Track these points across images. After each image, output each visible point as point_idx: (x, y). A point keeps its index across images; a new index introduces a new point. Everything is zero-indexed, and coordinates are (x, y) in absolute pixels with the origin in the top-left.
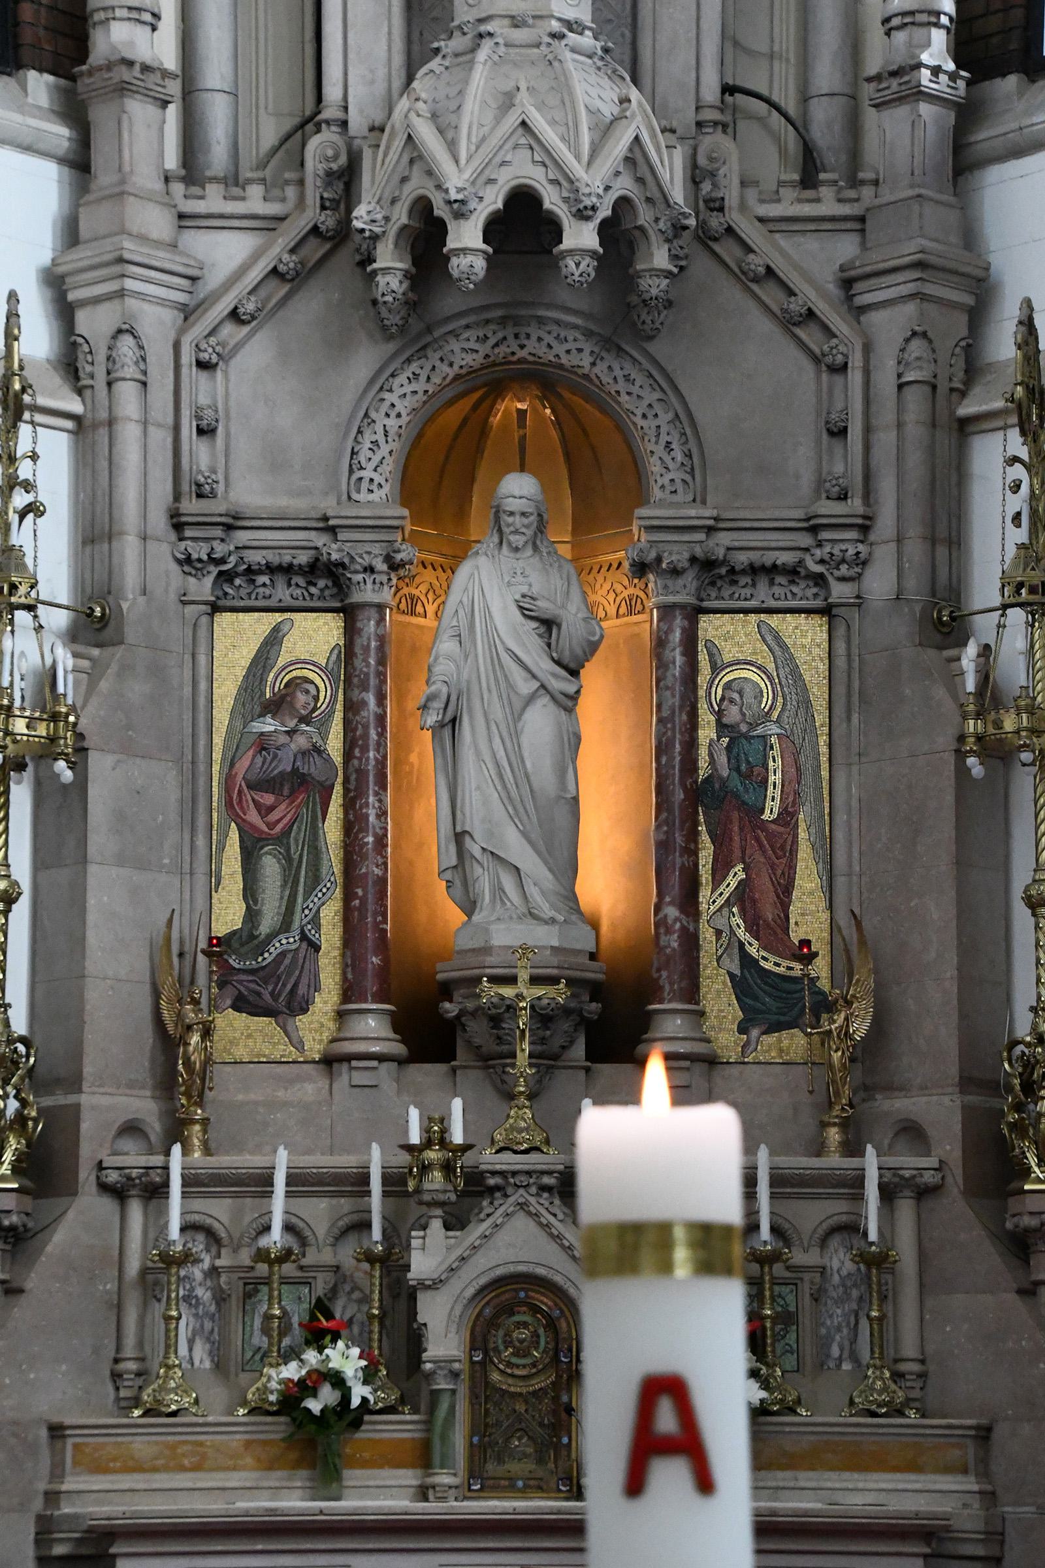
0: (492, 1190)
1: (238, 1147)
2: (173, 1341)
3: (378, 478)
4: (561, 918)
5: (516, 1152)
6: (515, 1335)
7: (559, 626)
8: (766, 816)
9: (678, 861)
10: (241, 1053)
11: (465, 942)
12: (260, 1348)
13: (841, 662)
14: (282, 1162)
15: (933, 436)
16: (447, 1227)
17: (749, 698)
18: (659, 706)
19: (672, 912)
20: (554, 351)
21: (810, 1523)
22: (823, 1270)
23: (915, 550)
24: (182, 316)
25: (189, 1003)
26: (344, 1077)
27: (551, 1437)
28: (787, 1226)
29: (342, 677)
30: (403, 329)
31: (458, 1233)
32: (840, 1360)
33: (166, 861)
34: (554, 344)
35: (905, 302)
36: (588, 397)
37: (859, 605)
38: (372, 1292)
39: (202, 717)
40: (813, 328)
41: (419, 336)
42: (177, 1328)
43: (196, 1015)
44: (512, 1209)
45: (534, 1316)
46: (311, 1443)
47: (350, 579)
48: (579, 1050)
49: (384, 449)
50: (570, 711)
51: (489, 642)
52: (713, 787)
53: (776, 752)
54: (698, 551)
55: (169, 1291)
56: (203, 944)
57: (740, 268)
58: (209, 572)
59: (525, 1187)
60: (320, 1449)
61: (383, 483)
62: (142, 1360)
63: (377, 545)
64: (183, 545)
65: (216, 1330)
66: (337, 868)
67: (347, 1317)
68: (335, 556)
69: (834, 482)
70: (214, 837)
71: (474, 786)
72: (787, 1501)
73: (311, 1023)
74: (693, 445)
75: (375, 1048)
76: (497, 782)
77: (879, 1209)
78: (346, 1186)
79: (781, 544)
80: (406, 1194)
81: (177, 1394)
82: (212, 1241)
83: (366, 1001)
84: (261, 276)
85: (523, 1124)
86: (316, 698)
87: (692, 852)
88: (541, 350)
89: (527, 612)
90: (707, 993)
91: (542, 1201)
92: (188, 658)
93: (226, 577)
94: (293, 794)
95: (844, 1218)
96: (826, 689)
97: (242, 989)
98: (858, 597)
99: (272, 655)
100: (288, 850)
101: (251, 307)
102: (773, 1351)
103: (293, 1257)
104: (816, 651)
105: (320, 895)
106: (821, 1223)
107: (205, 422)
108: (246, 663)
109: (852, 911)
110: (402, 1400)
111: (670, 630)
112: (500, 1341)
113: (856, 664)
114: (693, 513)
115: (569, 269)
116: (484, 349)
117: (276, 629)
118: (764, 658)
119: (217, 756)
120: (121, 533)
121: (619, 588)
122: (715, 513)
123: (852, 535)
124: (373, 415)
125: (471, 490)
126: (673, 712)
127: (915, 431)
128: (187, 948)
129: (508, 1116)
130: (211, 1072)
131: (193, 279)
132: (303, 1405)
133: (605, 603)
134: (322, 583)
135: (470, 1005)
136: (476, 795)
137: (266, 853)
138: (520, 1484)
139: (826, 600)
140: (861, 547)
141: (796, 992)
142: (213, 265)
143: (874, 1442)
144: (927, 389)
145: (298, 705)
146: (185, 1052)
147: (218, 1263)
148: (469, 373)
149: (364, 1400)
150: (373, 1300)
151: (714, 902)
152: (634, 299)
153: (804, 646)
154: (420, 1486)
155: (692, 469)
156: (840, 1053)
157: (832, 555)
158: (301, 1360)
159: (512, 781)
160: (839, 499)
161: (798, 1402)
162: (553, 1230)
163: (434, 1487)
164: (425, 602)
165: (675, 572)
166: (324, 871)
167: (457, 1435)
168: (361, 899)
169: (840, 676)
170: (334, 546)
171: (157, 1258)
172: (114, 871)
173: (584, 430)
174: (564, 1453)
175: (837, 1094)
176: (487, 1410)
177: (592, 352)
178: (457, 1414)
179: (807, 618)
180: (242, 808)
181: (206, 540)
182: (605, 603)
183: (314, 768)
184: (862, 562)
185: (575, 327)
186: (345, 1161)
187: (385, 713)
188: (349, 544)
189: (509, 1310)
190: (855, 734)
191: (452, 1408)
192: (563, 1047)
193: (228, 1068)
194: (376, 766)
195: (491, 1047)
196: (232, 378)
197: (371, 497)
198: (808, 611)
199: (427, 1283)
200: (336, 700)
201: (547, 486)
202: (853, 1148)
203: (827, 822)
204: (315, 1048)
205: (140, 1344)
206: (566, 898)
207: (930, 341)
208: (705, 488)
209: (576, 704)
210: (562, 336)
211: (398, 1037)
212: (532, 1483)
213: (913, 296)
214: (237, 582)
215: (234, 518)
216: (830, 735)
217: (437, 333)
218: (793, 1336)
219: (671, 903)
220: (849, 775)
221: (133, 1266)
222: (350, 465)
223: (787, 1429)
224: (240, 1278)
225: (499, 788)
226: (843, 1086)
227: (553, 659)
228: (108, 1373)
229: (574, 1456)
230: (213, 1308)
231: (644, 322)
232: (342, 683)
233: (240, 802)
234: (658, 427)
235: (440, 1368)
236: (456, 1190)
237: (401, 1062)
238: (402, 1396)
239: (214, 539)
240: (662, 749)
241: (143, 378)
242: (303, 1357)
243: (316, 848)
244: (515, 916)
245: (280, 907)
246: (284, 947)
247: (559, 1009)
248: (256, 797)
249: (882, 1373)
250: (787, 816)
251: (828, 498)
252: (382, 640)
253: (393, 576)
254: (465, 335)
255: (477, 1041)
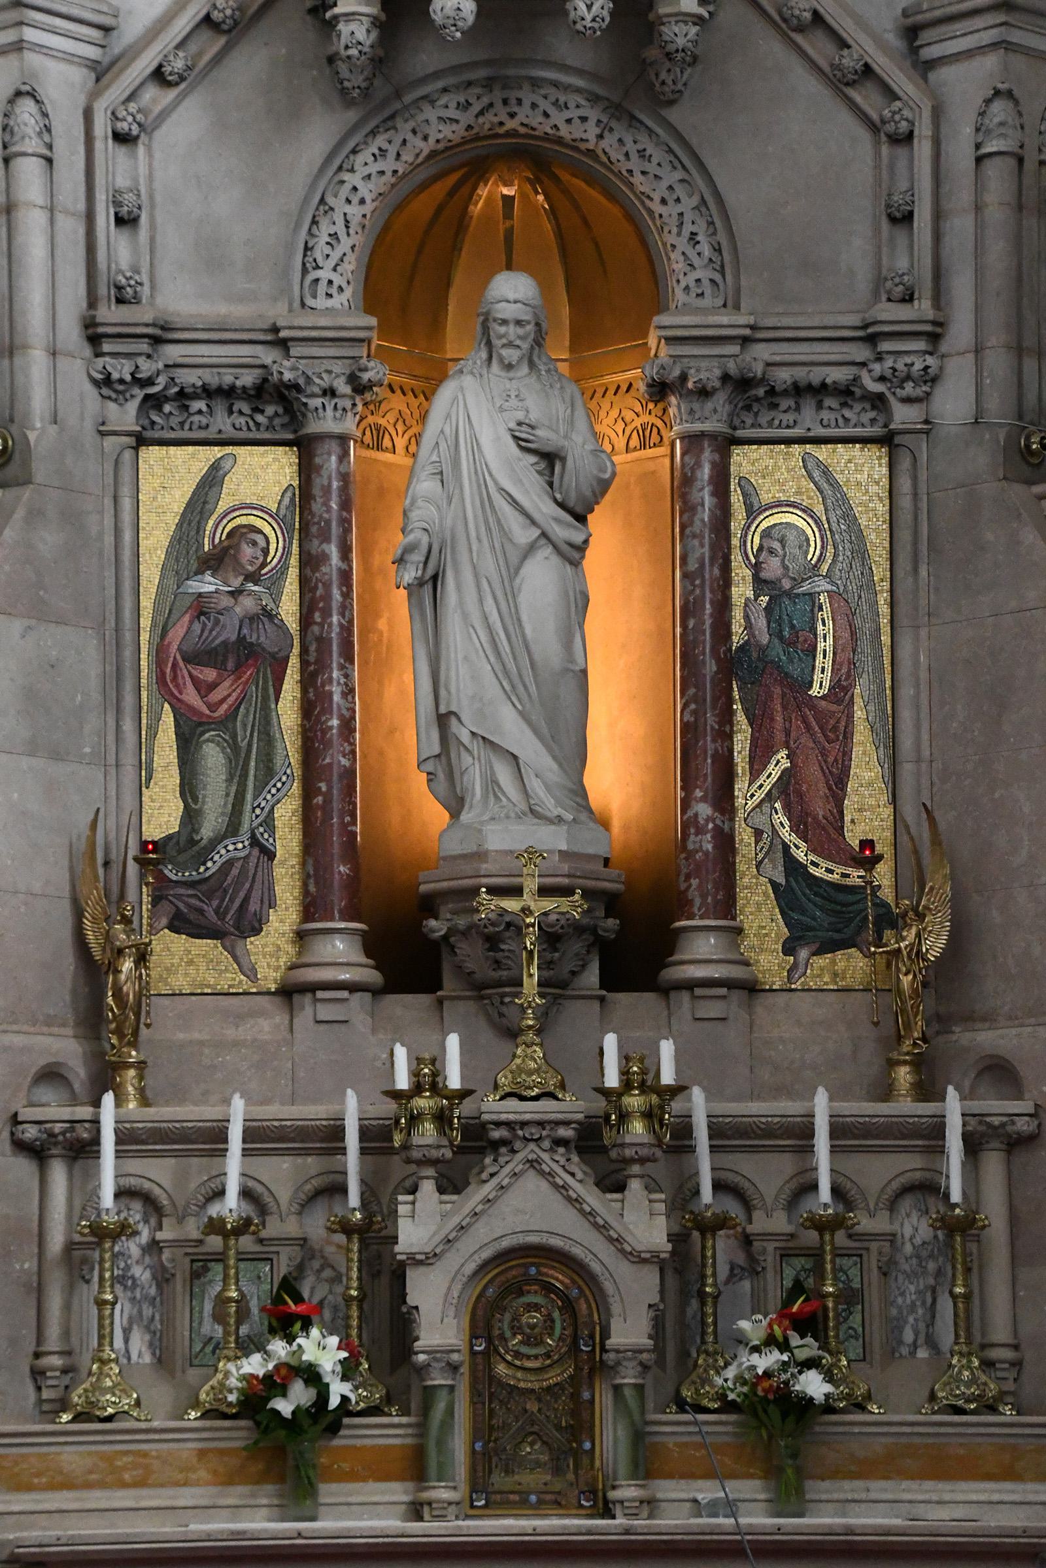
0: (495, 1145)
1: (180, 1095)
2: (108, 1330)
3: (338, 280)
4: (569, 817)
5: (523, 1098)
6: (524, 1320)
7: (563, 460)
8: (815, 691)
9: (710, 747)
10: (180, 982)
11: (453, 846)
12: (211, 1338)
13: (905, 502)
14: (238, 1112)
15: (1019, 224)
16: (441, 1190)
17: (792, 549)
18: (684, 559)
19: (704, 810)
20: (552, 121)
21: (892, 1542)
22: (892, 1238)
23: (998, 362)
24: (93, 76)
25: (120, 923)
26: (307, 1010)
27: (570, 1442)
28: (849, 1185)
29: (297, 524)
30: (366, 93)
31: (454, 1197)
32: (915, 1346)
33: (87, 750)
34: (551, 110)
35: (984, 53)
36: (592, 179)
37: (927, 432)
38: (349, 1269)
39: (127, 574)
40: (870, 87)
41: (385, 103)
42: (112, 1315)
43: (128, 937)
44: (521, 1166)
45: (546, 1296)
46: (280, 1451)
47: (305, 404)
48: (592, 977)
49: (345, 243)
50: (576, 564)
51: (478, 480)
52: (749, 657)
53: (826, 613)
54: (732, 367)
55: (102, 1270)
56: (133, 851)
57: (780, 13)
58: (132, 396)
59: (536, 1140)
60: (291, 1462)
61: (344, 285)
62: (68, 1353)
63: (339, 362)
64: (100, 361)
65: (157, 1317)
66: (295, 758)
67: (315, 1301)
68: (288, 376)
69: (897, 280)
70: (144, 721)
71: (460, 656)
72: (858, 1516)
73: (264, 946)
74: (722, 237)
75: (345, 976)
76: (489, 652)
77: (963, 1164)
78: (313, 1141)
79: (833, 358)
80: (391, 1151)
81: (114, 1395)
82: (151, 1209)
83: (332, 919)
84: (191, 25)
85: (532, 1065)
86: (266, 552)
87: (726, 735)
88: (536, 120)
89: (523, 444)
90: (744, 906)
91: (557, 1158)
92: (108, 502)
93: (153, 402)
94: (239, 667)
95: (918, 1175)
96: (886, 535)
97: (181, 906)
98: (927, 422)
99: (211, 498)
100: (234, 736)
101: (179, 64)
102: (837, 1336)
103: (253, 1228)
104: (873, 489)
105: (274, 791)
106: (890, 1181)
107: (126, 208)
108: (178, 507)
109: (924, 804)
110: (388, 1399)
111: (698, 464)
112: (506, 1326)
113: (924, 505)
114: (725, 320)
115: (579, 13)
116: (466, 118)
117: (215, 467)
118: (810, 498)
119: (146, 622)
120: (26, 347)
121: (629, 415)
122: (751, 320)
123: (921, 345)
124: (330, 200)
125: (446, 298)
126: (702, 565)
127: (997, 213)
128: (113, 856)
129: (514, 1056)
130: (148, 1005)
131: (106, 29)
132: (268, 1407)
133: (613, 435)
134: (270, 410)
135: (462, 922)
136: (463, 670)
137: (208, 740)
138: (533, 1498)
139: (886, 426)
140: (930, 360)
141: (858, 902)
142: (130, 12)
143: (961, 1445)
144: (1012, 162)
145: (244, 561)
146: (115, 982)
147: (160, 1236)
148: (447, 149)
149: (345, 1399)
150: (349, 1279)
151: (752, 796)
152: (652, 53)
153: (859, 484)
154: (413, 1503)
155: (722, 266)
156: (910, 977)
157: (894, 370)
158: (266, 1352)
159: (508, 649)
160: (903, 300)
161: (868, 1397)
162: (571, 1193)
163: (430, 1504)
164: (394, 433)
165: (704, 393)
166: (279, 761)
167: (457, 1441)
168: (324, 795)
169: (905, 517)
170: (286, 363)
171: (87, 1231)
172: (25, 762)
173: (586, 222)
174: (585, 1461)
175: (908, 1026)
176: (492, 1412)
177: (599, 121)
178: (456, 1416)
179: (862, 449)
180: (177, 686)
181: (128, 355)
182: (613, 435)
183: (264, 637)
184: (931, 379)
185: (578, 90)
186: (314, 1112)
187: (351, 568)
188: (303, 361)
189: (516, 1289)
190: (923, 594)
191: (450, 1411)
192: (573, 973)
193: (166, 1001)
194: (340, 634)
195: (486, 972)
196: (158, 155)
197: (330, 303)
198: (864, 441)
199: (418, 1257)
200: (290, 553)
201: (545, 286)
202: (928, 1090)
203: (889, 698)
204: (270, 975)
205: (66, 1334)
206: (572, 791)
207: (1016, 102)
208: (738, 291)
209: (583, 557)
210: (561, 102)
211: (371, 962)
212: (548, 1497)
213: (994, 45)
214: (167, 408)
215: (163, 328)
216: (892, 591)
217: (408, 98)
218: (858, 1317)
219: (704, 799)
220: (917, 638)
221: (56, 1241)
222: (304, 264)
223: (856, 1430)
224: (187, 1254)
225: (492, 659)
226: (916, 1016)
227: (555, 501)
228: (27, 1370)
229: (597, 1463)
230: (153, 1291)
231: (663, 83)
232: (296, 535)
233: (175, 678)
234: (681, 214)
235: (435, 1359)
236: (452, 1145)
237: (377, 992)
238: (388, 1393)
239: (140, 354)
240: (688, 611)
241: (48, 153)
242: (269, 1347)
243: (268, 735)
244: (513, 815)
245: (225, 804)
246: (231, 855)
247: (569, 925)
248: (195, 673)
249: (970, 1361)
250: (840, 691)
251: (889, 300)
252: (345, 478)
253: (358, 400)
254: (442, 102)
255: (470, 966)
